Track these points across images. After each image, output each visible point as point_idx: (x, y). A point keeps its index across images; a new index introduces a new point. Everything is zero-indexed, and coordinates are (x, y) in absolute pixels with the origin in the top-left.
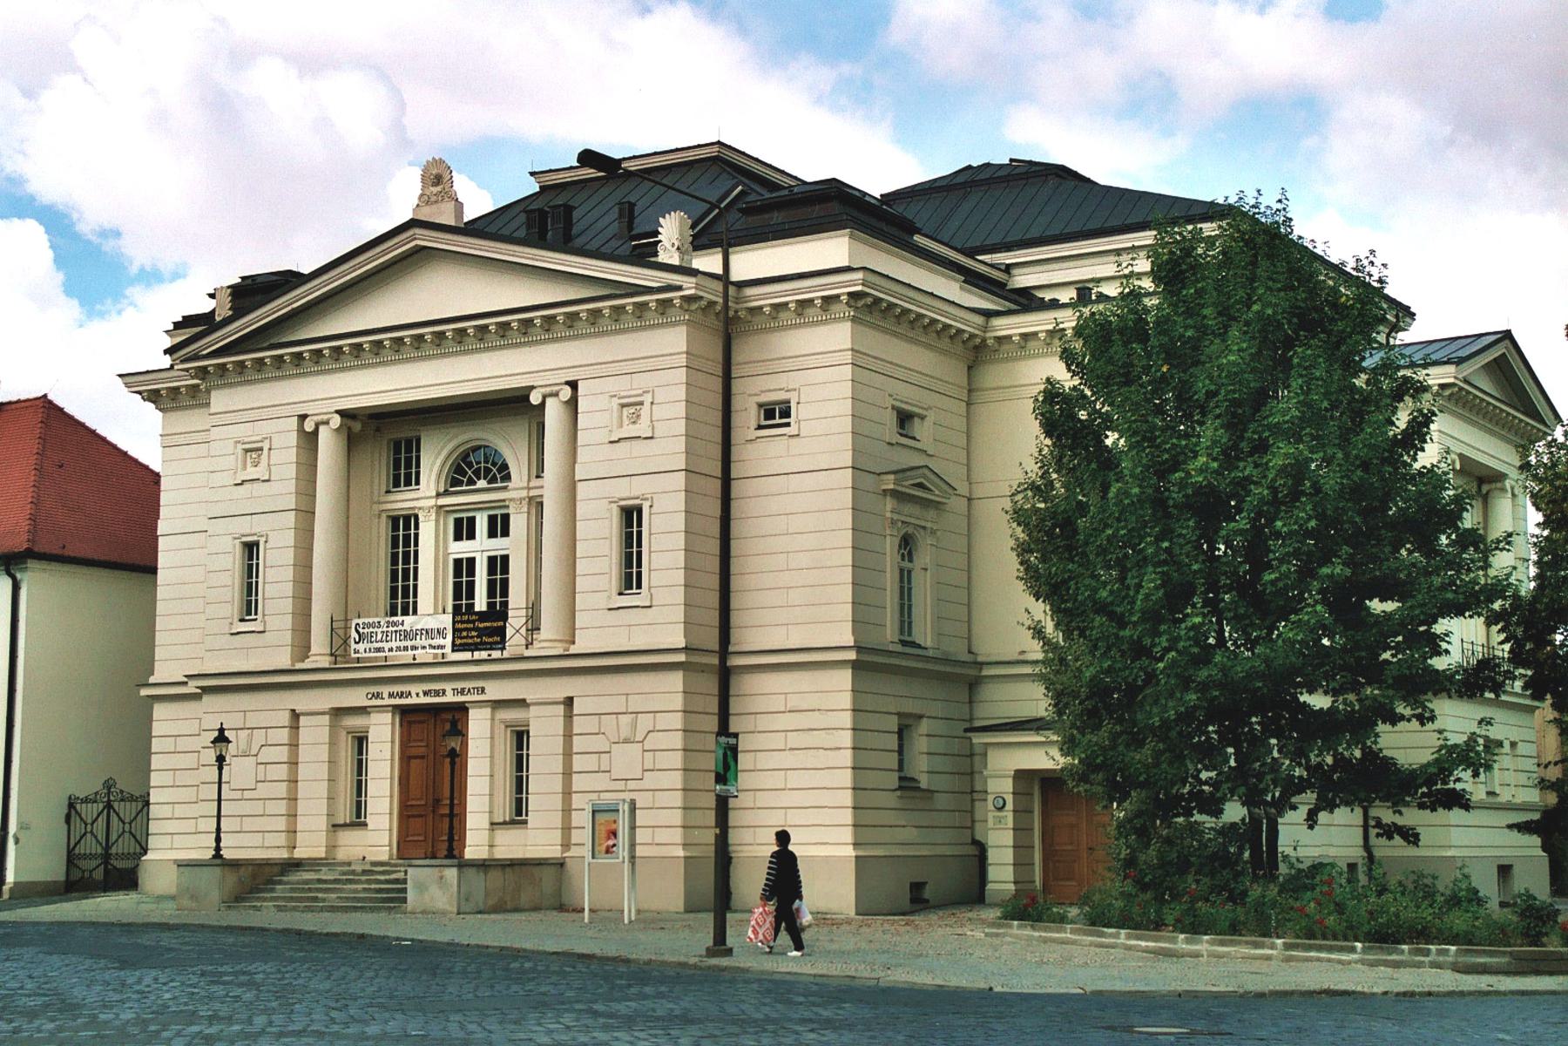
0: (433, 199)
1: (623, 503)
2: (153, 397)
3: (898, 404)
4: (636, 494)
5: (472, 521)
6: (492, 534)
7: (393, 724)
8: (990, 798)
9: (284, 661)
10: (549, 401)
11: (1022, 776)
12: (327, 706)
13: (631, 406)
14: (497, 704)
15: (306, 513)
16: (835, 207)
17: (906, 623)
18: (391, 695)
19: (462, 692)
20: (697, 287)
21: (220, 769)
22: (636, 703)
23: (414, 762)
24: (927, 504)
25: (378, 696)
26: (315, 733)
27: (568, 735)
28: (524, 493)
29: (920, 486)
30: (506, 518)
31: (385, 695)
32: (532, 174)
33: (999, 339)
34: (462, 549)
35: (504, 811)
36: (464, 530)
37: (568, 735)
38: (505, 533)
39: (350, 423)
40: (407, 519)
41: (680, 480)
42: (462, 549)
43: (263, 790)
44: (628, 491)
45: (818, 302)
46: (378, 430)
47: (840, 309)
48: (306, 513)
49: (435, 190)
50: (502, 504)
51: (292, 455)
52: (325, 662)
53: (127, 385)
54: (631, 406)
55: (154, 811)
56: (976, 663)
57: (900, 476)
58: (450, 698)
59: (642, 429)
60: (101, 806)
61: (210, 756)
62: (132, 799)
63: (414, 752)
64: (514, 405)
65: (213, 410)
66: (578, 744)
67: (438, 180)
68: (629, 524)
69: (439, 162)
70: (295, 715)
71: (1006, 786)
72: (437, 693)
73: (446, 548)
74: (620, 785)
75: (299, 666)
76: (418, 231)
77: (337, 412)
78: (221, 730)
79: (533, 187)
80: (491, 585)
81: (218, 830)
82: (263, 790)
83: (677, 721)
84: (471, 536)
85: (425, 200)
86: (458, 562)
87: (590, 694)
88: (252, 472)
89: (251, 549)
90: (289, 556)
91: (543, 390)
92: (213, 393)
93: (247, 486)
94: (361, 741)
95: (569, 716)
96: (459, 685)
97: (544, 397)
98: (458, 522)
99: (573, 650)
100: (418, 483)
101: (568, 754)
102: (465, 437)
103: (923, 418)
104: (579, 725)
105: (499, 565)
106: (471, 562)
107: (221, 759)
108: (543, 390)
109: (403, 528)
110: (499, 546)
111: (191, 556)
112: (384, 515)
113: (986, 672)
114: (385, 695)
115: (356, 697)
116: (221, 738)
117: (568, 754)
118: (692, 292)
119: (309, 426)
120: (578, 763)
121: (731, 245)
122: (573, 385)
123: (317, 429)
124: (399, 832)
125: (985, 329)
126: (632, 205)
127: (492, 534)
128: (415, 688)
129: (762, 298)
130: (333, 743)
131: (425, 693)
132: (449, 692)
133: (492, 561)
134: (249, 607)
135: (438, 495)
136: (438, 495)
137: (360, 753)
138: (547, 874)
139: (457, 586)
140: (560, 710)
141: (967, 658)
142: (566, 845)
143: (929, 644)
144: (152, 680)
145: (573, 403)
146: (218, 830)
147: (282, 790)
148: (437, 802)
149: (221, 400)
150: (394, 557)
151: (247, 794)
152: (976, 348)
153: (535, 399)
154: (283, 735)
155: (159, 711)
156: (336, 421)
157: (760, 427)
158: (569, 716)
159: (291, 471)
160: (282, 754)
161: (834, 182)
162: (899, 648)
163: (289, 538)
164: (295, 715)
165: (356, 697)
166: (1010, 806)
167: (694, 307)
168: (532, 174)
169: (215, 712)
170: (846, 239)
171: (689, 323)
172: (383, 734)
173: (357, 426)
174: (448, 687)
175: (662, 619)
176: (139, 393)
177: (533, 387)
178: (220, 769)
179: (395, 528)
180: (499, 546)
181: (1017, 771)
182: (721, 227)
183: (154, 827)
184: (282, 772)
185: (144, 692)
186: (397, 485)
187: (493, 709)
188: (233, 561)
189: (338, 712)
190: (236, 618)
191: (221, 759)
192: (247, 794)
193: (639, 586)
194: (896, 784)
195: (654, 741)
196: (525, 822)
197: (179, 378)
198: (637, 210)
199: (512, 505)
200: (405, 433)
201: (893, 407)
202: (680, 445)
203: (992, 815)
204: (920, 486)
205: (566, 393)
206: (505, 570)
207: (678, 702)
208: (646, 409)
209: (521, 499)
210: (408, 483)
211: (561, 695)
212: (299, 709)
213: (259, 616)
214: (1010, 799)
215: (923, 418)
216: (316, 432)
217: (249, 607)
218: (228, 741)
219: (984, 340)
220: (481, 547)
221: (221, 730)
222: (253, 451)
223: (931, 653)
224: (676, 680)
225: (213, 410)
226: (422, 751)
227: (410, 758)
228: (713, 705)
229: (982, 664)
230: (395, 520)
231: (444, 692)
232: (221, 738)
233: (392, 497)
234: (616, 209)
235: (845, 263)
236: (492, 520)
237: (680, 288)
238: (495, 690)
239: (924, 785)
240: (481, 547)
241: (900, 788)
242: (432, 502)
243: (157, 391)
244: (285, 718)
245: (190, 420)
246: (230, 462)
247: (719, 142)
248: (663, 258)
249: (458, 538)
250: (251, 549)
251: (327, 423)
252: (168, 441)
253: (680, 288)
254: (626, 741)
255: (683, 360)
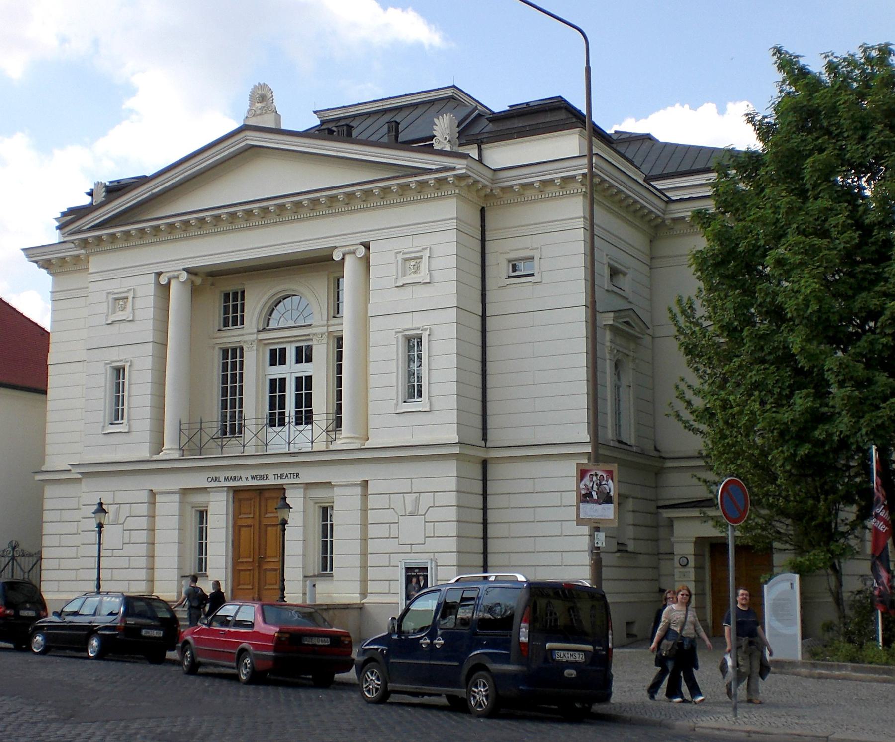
0: (258, 112)
1: (407, 333)
2: (46, 265)
3: (612, 262)
4: (418, 326)
5: (283, 351)
6: (299, 360)
7: (227, 501)
8: (677, 558)
9: (145, 454)
10: (347, 258)
11: (700, 541)
12: (176, 487)
13: (412, 261)
14: (308, 486)
15: (162, 344)
16: (562, 115)
17: (618, 426)
18: (226, 479)
19: (281, 477)
20: (468, 167)
21: (100, 532)
22: (418, 485)
23: (243, 529)
24: (635, 339)
25: (216, 479)
26: (168, 507)
27: (365, 510)
28: (324, 329)
29: (627, 323)
30: (310, 348)
31: (222, 479)
32: (315, 112)
33: (675, 220)
34: (277, 372)
35: (315, 566)
36: (277, 357)
37: (365, 510)
38: (309, 359)
39: (194, 278)
40: (234, 350)
41: (453, 314)
42: (277, 372)
43: (129, 550)
44: (410, 324)
45: (558, 181)
46: (213, 285)
47: (576, 187)
48: (162, 344)
49: (259, 105)
50: (308, 337)
51: (150, 301)
52: (176, 455)
53: (28, 256)
54: (412, 261)
55: (45, 564)
56: (661, 457)
57: (617, 315)
58: (272, 481)
59: (423, 275)
60: (7, 559)
61: (93, 524)
62: (31, 555)
63: (243, 522)
64: (322, 263)
65: (90, 271)
66: (372, 516)
67: (263, 98)
68: (410, 348)
69: (263, 86)
70: (152, 494)
71: (688, 549)
72: (262, 478)
73: (264, 371)
74: (408, 548)
75: (155, 457)
76: (248, 133)
77: (184, 269)
78: (101, 504)
79: (318, 122)
80: (298, 398)
81: (99, 579)
82: (129, 550)
83: (452, 499)
84: (283, 362)
85: (252, 113)
86: (273, 382)
87: (383, 480)
88: (120, 315)
89: (119, 371)
90: (148, 377)
91: (343, 249)
92: (91, 259)
93: (117, 326)
94: (202, 515)
95: (365, 495)
96: (279, 472)
97: (344, 255)
98: (273, 352)
99: (368, 445)
100: (242, 323)
101: (365, 524)
102: (278, 289)
103: (625, 274)
104: (372, 502)
105: (305, 384)
106: (283, 381)
107: (100, 526)
108: (343, 249)
109: (232, 359)
110: (304, 370)
111: (74, 381)
112: (217, 348)
113: (669, 464)
114: (222, 479)
115: (199, 481)
116: (101, 509)
117: (365, 524)
118: (464, 171)
119: (163, 280)
120: (373, 531)
121: (482, 142)
122: (367, 246)
123: (169, 283)
124: (233, 581)
125: (664, 212)
126: (398, 124)
127: (299, 360)
128: (244, 474)
129: (514, 180)
130: (181, 515)
131: (253, 478)
132: (271, 477)
133: (299, 380)
134: (117, 416)
135: (259, 331)
136: (259, 331)
137: (201, 522)
138: (353, 615)
139: (272, 399)
140: (359, 490)
141: (655, 453)
142: (364, 594)
143: (632, 441)
144: (44, 469)
145: (366, 261)
146: (99, 579)
147: (143, 549)
148: (261, 560)
149: (96, 263)
150: (225, 378)
151: (116, 553)
152: (657, 227)
153: (337, 256)
154: (144, 509)
155: (49, 491)
156: (184, 276)
157: (509, 277)
158: (365, 495)
159: (150, 313)
160: (143, 523)
161: (560, 99)
162: (617, 444)
163: (148, 362)
164: (152, 494)
165: (199, 481)
166: (692, 564)
167: (463, 183)
168: (315, 112)
169: (90, 494)
170: (577, 136)
171: (459, 196)
172: (219, 511)
173: (198, 281)
174: (271, 473)
175: (439, 421)
176: (36, 262)
177: (336, 247)
178: (100, 532)
179: (225, 357)
180: (304, 370)
181: (697, 538)
182: (476, 130)
183: (45, 575)
184: (143, 536)
185: (38, 477)
186: (226, 324)
187: (305, 489)
188: (103, 381)
189: (185, 492)
190: (107, 421)
191: (100, 526)
192: (116, 553)
193: (420, 396)
194: (615, 548)
195: (433, 515)
196: (331, 576)
197: (66, 250)
198: (401, 128)
199: (315, 338)
200: (232, 287)
201: (609, 265)
202: (453, 288)
203: (678, 571)
204: (627, 323)
205: (362, 251)
206: (309, 386)
207: (452, 484)
208: (425, 260)
209: (322, 334)
210: (235, 323)
211: (359, 480)
212: (155, 489)
213: (125, 421)
214: (691, 559)
215: (625, 274)
216: (167, 286)
217: (117, 416)
218: (105, 512)
219: (664, 221)
220: (290, 371)
221: (101, 504)
222: (120, 300)
223: (635, 449)
224: (177, 495)
225: (90, 271)
226: (249, 522)
227: (241, 526)
228: (478, 487)
229: (664, 458)
230: (225, 352)
231: (267, 477)
232: (101, 509)
233: (223, 334)
234: (386, 128)
235: (578, 155)
236: (299, 350)
237: (454, 169)
238: (308, 476)
239: (631, 548)
240: (290, 371)
241: (619, 551)
242: (254, 337)
243: (49, 260)
244: (144, 496)
245: (73, 281)
246: (103, 308)
247: (454, 86)
248: (437, 146)
249: (273, 363)
250: (119, 371)
251: (177, 277)
252: (57, 297)
253: (454, 169)
254: (411, 514)
255: (454, 224)
